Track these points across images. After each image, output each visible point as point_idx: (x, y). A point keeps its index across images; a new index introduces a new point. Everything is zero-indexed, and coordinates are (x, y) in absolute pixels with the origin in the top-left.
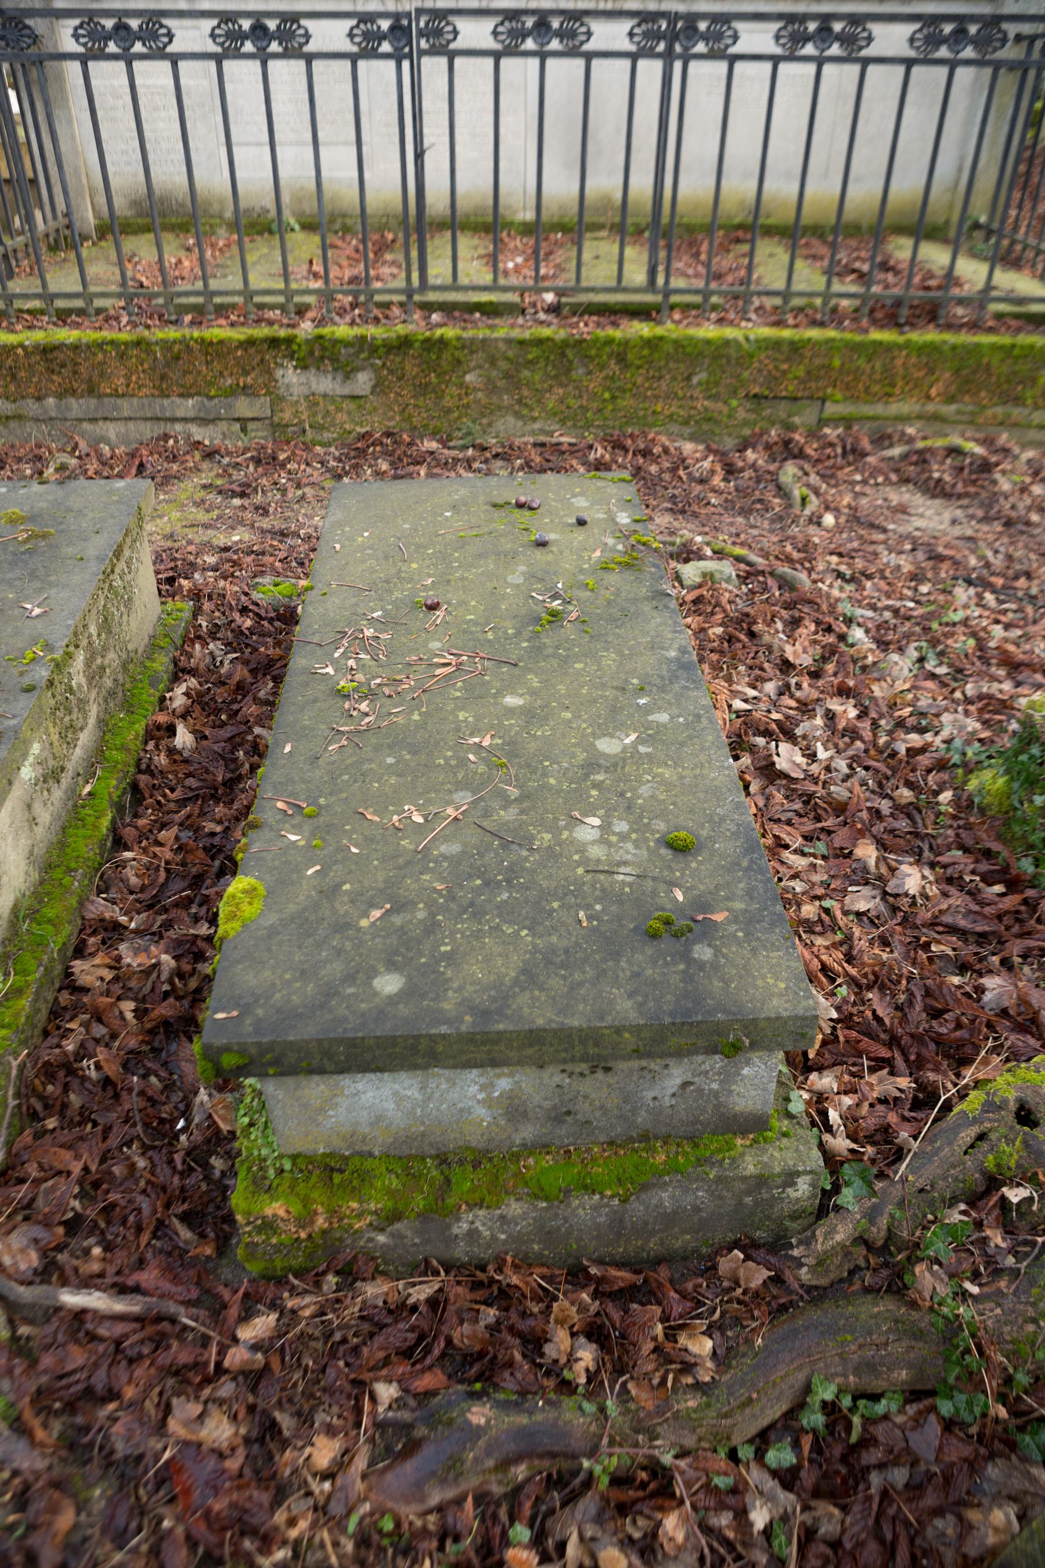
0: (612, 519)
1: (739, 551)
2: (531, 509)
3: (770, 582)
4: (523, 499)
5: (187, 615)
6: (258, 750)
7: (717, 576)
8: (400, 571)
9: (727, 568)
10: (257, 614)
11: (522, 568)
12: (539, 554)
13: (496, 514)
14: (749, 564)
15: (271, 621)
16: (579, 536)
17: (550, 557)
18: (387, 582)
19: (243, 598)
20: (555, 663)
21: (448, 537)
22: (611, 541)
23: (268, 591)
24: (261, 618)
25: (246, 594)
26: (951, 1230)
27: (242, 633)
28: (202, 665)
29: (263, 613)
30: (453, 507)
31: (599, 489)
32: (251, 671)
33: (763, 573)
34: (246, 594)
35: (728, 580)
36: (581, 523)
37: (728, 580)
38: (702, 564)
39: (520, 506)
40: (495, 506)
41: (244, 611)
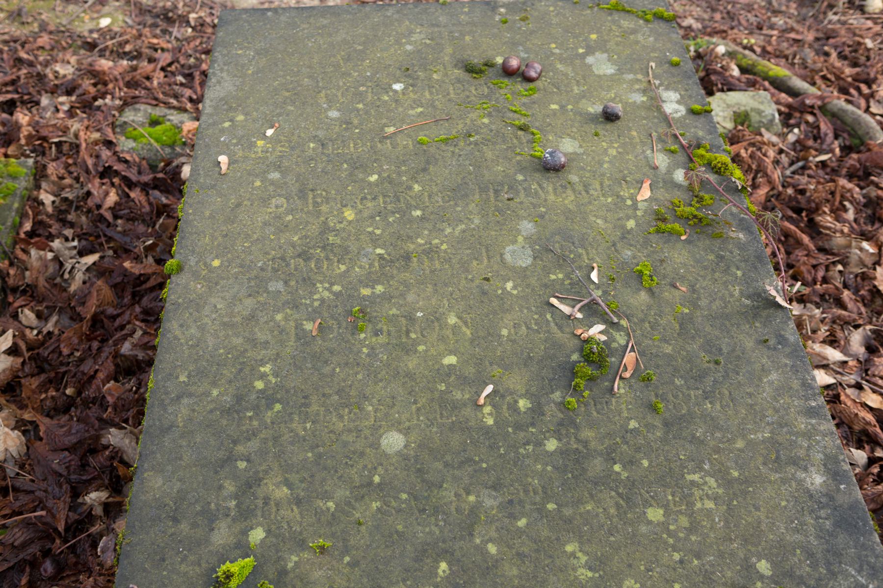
0: (655, 104)
1: (779, 70)
2: (530, 80)
3: (825, 127)
4: (514, 63)
5: (23, 184)
6: (117, 477)
7: (754, 118)
8: (325, 229)
9: (762, 104)
10: (125, 179)
11: (527, 227)
12: (548, 189)
13: (477, 88)
14: (793, 93)
15: (145, 188)
16: (609, 146)
17: (569, 199)
18: (304, 256)
19: (106, 153)
20: (609, 499)
21: (403, 141)
22: (661, 160)
23: (140, 133)
24: (131, 184)
25: (109, 144)
26: (808, 565)
27: (101, 219)
28: (42, 282)
29: (133, 175)
30: (406, 72)
31: (626, 34)
32: (114, 286)
33: (811, 110)
34: (109, 144)
35: (769, 126)
36: (610, 117)
37: (769, 126)
38: (734, 97)
39: (508, 72)
40: (471, 70)
41: (106, 173)
